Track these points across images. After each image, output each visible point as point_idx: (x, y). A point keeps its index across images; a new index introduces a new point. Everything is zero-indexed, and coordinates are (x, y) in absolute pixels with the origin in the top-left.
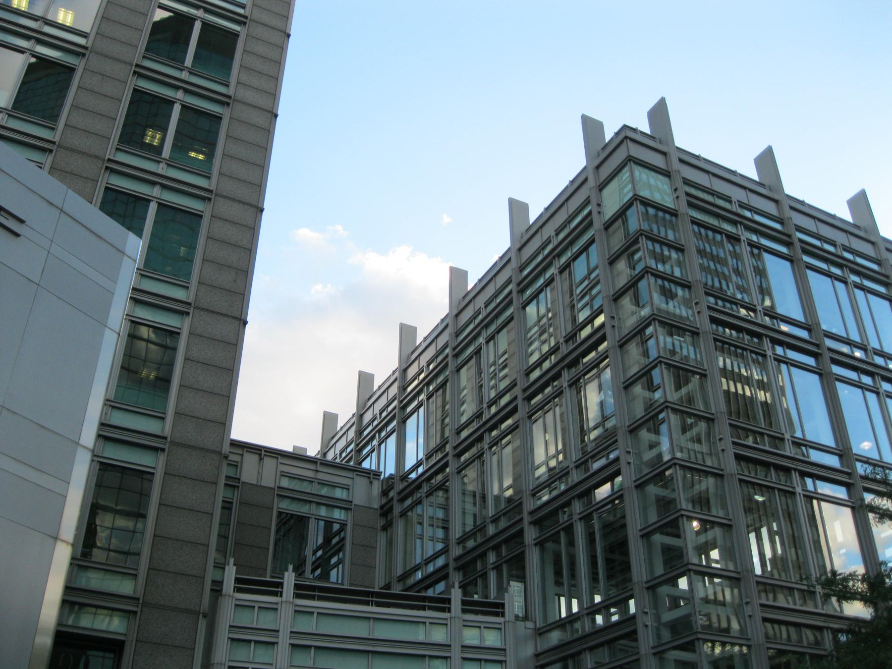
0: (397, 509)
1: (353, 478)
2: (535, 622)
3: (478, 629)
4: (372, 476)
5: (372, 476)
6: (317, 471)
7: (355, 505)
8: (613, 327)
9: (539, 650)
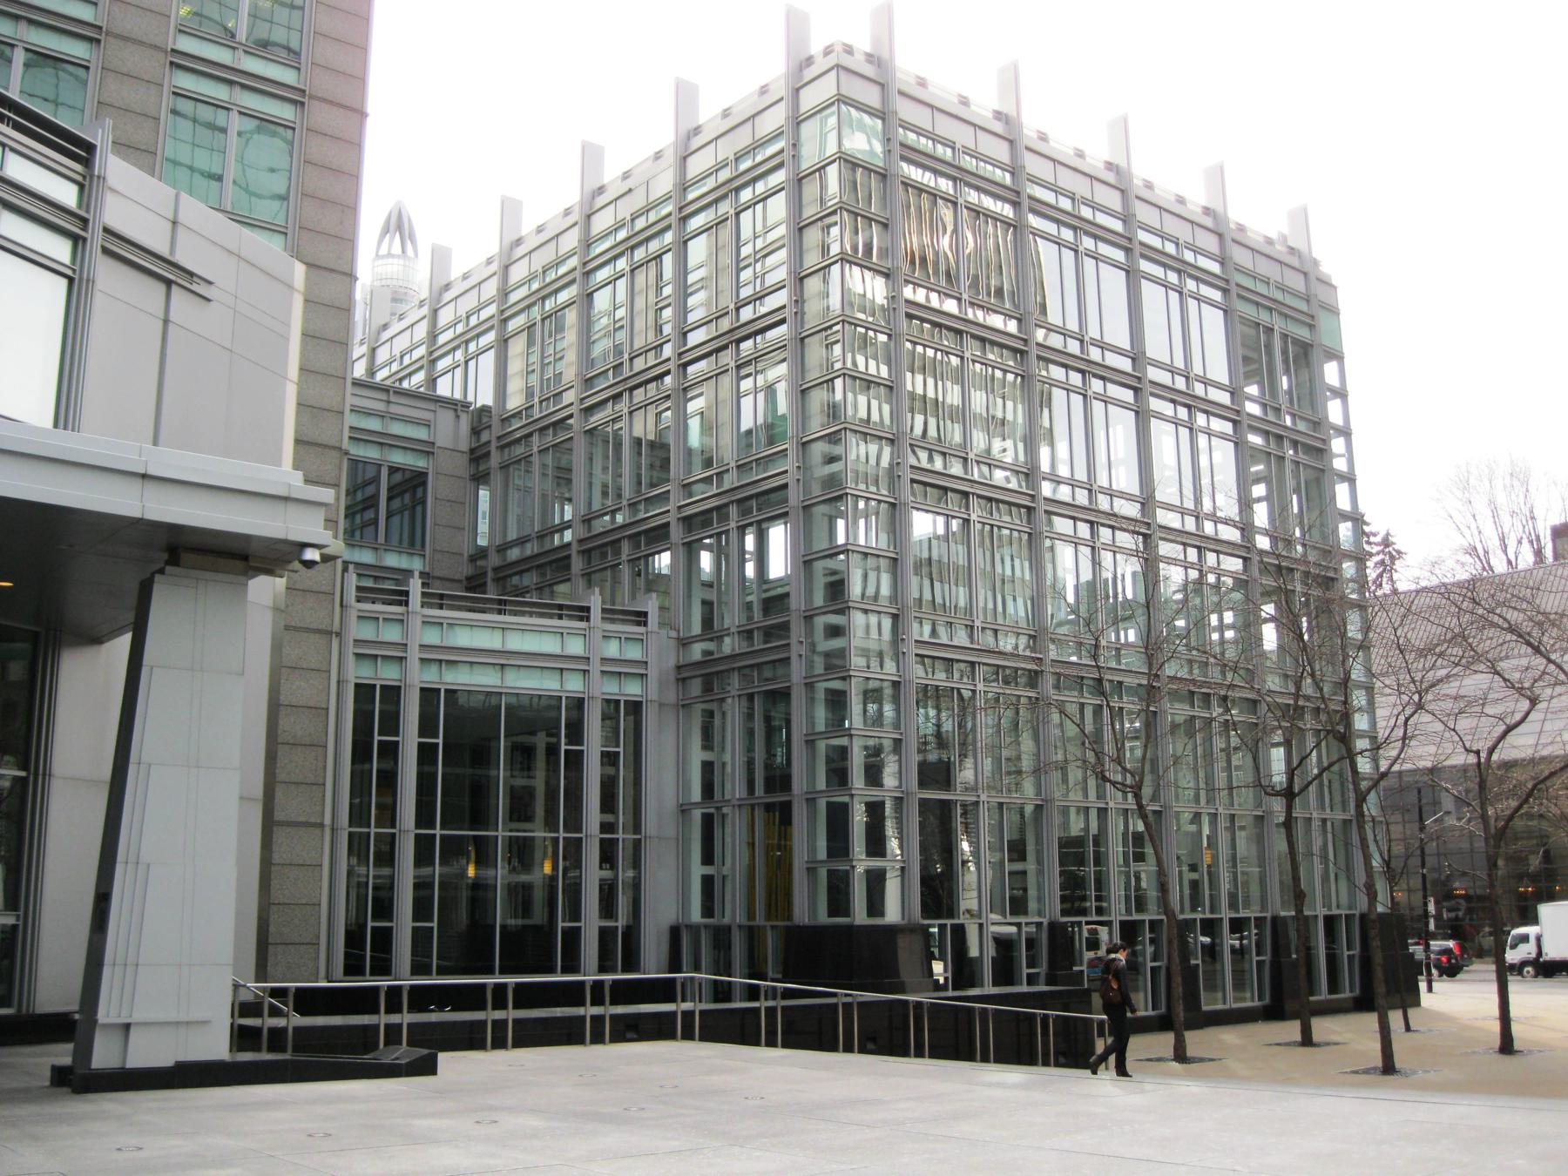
0: (495, 459)
1: (435, 411)
2: (679, 631)
3: (283, 237)
4: (459, 408)
5: (459, 408)
6: (389, 402)
7: (439, 447)
8: (801, 656)
9: (681, 663)
